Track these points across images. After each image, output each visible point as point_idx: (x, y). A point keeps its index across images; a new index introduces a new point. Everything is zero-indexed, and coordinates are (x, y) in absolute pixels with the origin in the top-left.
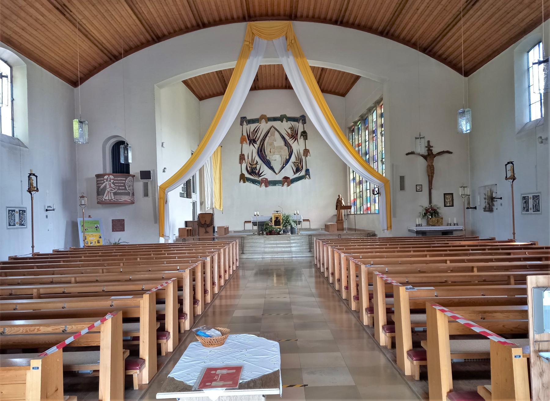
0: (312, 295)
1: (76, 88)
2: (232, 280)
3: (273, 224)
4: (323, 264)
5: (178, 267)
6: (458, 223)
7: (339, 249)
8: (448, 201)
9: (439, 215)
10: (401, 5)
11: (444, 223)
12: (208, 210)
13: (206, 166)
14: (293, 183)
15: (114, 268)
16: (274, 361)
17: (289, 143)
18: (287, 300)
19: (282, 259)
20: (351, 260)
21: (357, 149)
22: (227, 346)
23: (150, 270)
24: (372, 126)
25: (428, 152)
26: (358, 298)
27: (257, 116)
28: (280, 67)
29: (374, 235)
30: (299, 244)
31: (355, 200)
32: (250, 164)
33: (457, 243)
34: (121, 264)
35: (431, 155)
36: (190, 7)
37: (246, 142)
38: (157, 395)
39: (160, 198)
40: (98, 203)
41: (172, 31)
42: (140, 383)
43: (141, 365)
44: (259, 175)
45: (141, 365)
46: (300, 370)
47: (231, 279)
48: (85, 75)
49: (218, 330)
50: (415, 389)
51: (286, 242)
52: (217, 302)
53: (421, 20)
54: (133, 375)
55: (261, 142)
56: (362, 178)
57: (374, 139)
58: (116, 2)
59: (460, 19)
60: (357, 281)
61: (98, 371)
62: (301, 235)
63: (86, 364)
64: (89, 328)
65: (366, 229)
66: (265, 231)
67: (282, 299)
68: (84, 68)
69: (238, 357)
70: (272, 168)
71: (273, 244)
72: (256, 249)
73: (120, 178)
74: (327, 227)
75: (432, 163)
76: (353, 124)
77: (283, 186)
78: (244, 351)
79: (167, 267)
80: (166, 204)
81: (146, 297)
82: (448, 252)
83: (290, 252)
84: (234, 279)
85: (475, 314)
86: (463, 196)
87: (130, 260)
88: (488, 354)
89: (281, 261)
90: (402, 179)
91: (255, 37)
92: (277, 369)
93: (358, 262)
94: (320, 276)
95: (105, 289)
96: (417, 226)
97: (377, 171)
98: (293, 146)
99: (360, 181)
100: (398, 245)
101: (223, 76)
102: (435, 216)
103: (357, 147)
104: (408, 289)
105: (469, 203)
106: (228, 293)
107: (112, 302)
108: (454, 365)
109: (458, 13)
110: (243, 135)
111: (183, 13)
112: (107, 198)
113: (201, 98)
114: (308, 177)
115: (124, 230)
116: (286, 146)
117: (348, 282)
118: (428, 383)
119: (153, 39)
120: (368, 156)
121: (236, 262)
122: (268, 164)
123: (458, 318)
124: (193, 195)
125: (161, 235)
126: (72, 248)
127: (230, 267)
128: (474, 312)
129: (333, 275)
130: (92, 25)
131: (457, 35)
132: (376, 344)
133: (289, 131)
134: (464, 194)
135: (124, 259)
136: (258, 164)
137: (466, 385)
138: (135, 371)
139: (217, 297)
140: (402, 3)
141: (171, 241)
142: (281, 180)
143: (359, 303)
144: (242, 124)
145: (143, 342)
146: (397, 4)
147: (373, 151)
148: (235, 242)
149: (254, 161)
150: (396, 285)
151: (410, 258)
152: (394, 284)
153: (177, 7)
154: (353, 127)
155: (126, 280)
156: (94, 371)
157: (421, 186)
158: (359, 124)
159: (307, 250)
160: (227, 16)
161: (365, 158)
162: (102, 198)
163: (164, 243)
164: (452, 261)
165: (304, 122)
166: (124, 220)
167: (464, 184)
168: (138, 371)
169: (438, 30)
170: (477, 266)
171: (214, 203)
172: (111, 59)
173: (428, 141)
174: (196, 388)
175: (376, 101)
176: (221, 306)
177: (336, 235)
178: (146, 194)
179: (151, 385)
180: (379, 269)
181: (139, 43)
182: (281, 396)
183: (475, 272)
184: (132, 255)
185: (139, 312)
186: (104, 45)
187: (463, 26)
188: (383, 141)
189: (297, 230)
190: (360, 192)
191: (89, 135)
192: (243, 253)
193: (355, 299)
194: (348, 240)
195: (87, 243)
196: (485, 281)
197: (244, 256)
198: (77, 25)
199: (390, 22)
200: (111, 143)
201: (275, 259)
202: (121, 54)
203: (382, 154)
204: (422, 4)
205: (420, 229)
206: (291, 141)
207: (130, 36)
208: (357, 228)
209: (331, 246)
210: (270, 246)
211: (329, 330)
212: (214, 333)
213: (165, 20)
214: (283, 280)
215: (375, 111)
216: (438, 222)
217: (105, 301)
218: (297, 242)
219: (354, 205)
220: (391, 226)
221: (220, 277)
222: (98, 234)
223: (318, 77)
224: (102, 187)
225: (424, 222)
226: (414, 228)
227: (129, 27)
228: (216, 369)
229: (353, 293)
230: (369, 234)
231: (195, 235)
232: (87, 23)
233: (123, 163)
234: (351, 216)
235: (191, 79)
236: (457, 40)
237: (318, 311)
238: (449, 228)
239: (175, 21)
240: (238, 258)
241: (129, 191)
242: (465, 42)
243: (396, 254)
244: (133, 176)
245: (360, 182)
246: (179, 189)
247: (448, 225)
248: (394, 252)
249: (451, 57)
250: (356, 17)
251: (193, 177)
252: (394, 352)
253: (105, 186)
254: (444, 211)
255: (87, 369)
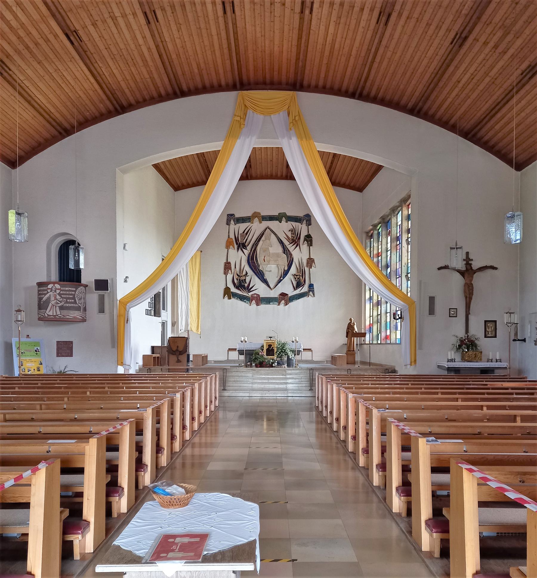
0: (311, 446)
1: (15, 170)
2: (208, 424)
3: (265, 354)
4: (326, 407)
5: (138, 405)
6: (501, 360)
7: (346, 388)
8: (490, 330)
9: (478, 347)
10: (438, 76)
11: (484, 358)
12: (182, 333)
13: (181, 276)
14: (292, 301)
15: (55, 404)
16: (250, 528)
17: (289, 251)
18: (279, 451)
19: (274, 399)
20: (360, 402)
21: (375, 260)
22: (192, 508)
23: (102, 408)
24: (395, 231)
25: (466, 267)
26: (367, 451)
27: (249, 214)
28: (280, 151)
29: (394, 371)
30: (297, 380)
31: (371, 326)
32: (237, 274)
33: (499, 384)
34: (65, 398)
35: (470, 271)
36: (165, 69)
37: (234, 247)
38: (96, 567)
39: (120, 316)
40: (40, 319)
41: (141, 100)
42: (83, 552)
43: (83, 529)
44: (249, 290)
45: (85, 529)
46: (289, 540)
47: (207, 422)
48: (26, 153)
49: (182, 487)
50: (434, 569)
51: (280, 377)
52: (188, 451)
53: (463, 96)
54: (73, 541)
55: (252, 247)
56: (381, 298)
57: (398, 248)
58: (70, 60)
59: (512, 97)
60: (367, 430)
61: (27, 534)
62: (300, 368)
63: (12, 525)
64: (16, 480)
65: (383, 363)
66: (254, 362)
67: (271, 450)
68: (25, 143)
69: (205, 522)
70: (265, 282)
71: (264, 379)
72: (242, 385)
73: (69, 288)
74: (334, 359)
75: (471, 280)
76: (371, 227)
77: (279, 305)
78: (213, 515)
79: (124, 405)
80: (127, 323)
81: (93, 442)
82: (486, 396)
83: (286, 390)
84: (211, 422)
85: (513, 476)
86: (509, 325)
87: (78, 394)
88: (524, 526)
89: (273, 401)
90: (432, 300)
91: (248, 111)
92: (252, 539)
93: (369, 405)
94: (321, 421)
95: (42, 430)
96: (448, 361)
97: (400, 289)
98: (293, 253)
99: (378, 301)
100: (423, 384)
101: (205, 160)
102: (472, 349)
103: (376, 258)
104: (430, 441)
105: (516, 334)
106: (203, 440)
107: (49, 447)
108: (483, 540)
109: (511, 88)
110: (230, 237)
111: (156, 76)
112: (51, 313)
113: (176, 188)
114: (312, 295)
115: (71, 355)
116: (284, 253)
117: (356, 430)
118: (449, 562)
119: (116, 109)
120: (389, 269)
121: (215, 401)
122: (261, 275)
123: (490, 480)
124: (163, 312)
125: (120, 363)
126: (4, 376)
127: (206, 407)
128: (511, 473)
129: (338, 421)
130: (38, 88)
131: (508, 116)
132: (388, 510)
133: (290, 234)
134: (510, 322)
135: (70, 392)
136: (248, 276)
137: (497, 565)
138: (76, 536)
139: (188, 445)
140: (440, 72)
141: (132, 371)
142: (276, 296)
143: (368, 457)
144: (228, 223)
145: (88, 499)
146: (432, 73)
147: (397, 263)
148: (214, 375)
149: (242, 272)
150: (414, 436)
151: (437, 401)
152: (412, 434)
153: (148, 69)
154: (372, 232)
155: (70, 420)
156: (23, 535)
157: (455, 310)
158: (380, 228)
159: (306, 388)
160: (213, 83)
161: (386, 272)
162: (44, 313)
163: (123, 373)
164: (489, 408)
165: (309, 223)
166: (72, 342)
167: (510, 309)
168: (80, 536)
169: (484, 109)
170: (520, 414)
171: (189, 323)
172: (60, 133)
173: (467, 252)
174: (147, 560)
175: (402, 199)
176: (193, 456)
177: (345, 370)
178: (102, 310)
179: (97, 554)
180: (395, 414)
181: (97, 114)
182: (258, 573)
183: (517, 422)
184: (80, 388)
185: (84, 462)
186: (51, 115)
187: (516, 106)
188: (409, 250)
189: (296, 361)
190: (378, 315)
191: (29, 230)
192: (224, 390)
193: (364, 453)
194: (359, 376)
195: (24, 370)
196: (529, 434)
197: (226, 394)
198: (18, 87)
199: (422, 97)
200: (58, 242)
201: (265, 398)
202: (73, 127)
203: (408, 267)
204: (465, 74)
205: (452, 365)
206: (291, 248)
207: (86, 104)
208: (372, 361)
209: (337, 384)
210: (260, 381)
211: (329, 491)
212: (176, 490)
213: (133, 85)
214: (276, 426)
215: (401, 212)
216: (475, 357)
217: (40, 445)
218: (294, 377)
219: (370, 332)
220: (415, 361)
221: (193, 419)
222: (38, 359)
223: (328, 166)
224: (44, 299)
225: (458, 357)
226: (445, 364)
227: (85, 92)
228: (174, 537)
229: (362, 444)
230: (387, 369)
231: (164, 364)
232: (30, 85)
233: (73, 268)
234: (365, 346)
235: (164, 163)
236: (508, 123)
237: (317, 466)
238: (489, 365)
239: (145, 87)
240: (217, 396)
241: (79, 305)
242: (518, 125)
243: (420, 396)
244: (86, 286)
245: (379, 303)
246: (145, 304)
247: (488, 361)
248: (417, 393)
249: (501, 145)
250: (379, 89)
251: (164, 289)
252: (409, 521)
253: (49, 298)
254: (484, 343)
255: (14, 532)
